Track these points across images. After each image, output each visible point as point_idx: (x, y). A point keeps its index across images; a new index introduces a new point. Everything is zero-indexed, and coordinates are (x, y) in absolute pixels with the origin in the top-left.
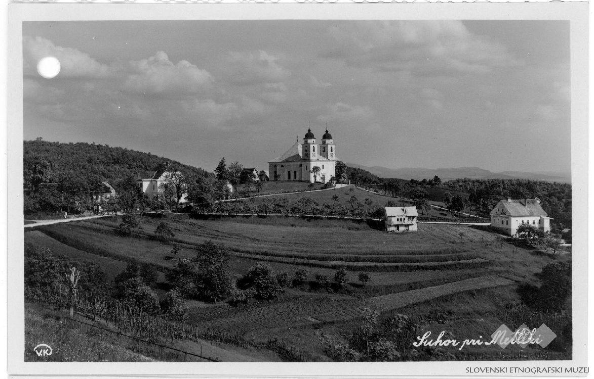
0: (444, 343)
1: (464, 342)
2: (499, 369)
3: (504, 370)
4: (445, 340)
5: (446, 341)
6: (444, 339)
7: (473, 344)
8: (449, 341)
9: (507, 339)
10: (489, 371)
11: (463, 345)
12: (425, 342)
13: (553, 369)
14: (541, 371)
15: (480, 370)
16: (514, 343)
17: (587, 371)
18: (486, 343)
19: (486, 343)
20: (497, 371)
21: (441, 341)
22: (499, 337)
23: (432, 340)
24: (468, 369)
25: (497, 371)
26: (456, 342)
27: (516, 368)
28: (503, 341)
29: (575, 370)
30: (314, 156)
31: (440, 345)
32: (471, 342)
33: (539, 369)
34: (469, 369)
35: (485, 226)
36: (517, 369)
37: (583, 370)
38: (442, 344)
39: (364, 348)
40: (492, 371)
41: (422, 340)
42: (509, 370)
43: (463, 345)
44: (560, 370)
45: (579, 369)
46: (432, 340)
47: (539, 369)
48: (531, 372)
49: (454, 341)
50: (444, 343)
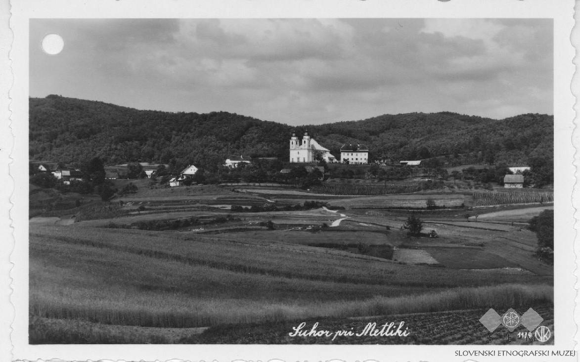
0: (318, 334)
1: (337, 333)
2: (488, 353)
3: (493, 353)
4: (319, 331)
5: (319, 332)
6: (317, 330)
7: (345, 335)
8: (323, 332)
9: (377, 331)
10: (478, 354)
11: (336, 335)
12: (300, 333)
13: (540, 352)
14: (528, 354)
15: (469, 353)
16: (383, 335)
17: (573, 354)
18: (357, 335)
19: (357, 335)
20: (485, 354)
21: (315, 331)
22: (369, 329)
23: (306, 331)
24: (457, 352)
25: (485, 354)
26: (352, 333)
27: (503, 351)
28: (373, 333)
29: (562, 354)
30: (292, 147)
31: (315, 335)
32: (343, 333)
33: (526, 352)
34: (458, 352)
35: (493, 219)
36: (505, 353)
37: (569, 354)
38: (316, 335)
39: (421, 335)
40: (482, 353)
41: (297, 330)
42: (497, 353)
43: (336, 335)
44: (546, 353)
45: (566, 353)
46: (306, 331)
47: (526, 352)
48: (518, 355)
49: (327, 332)
50: (318, 334)
